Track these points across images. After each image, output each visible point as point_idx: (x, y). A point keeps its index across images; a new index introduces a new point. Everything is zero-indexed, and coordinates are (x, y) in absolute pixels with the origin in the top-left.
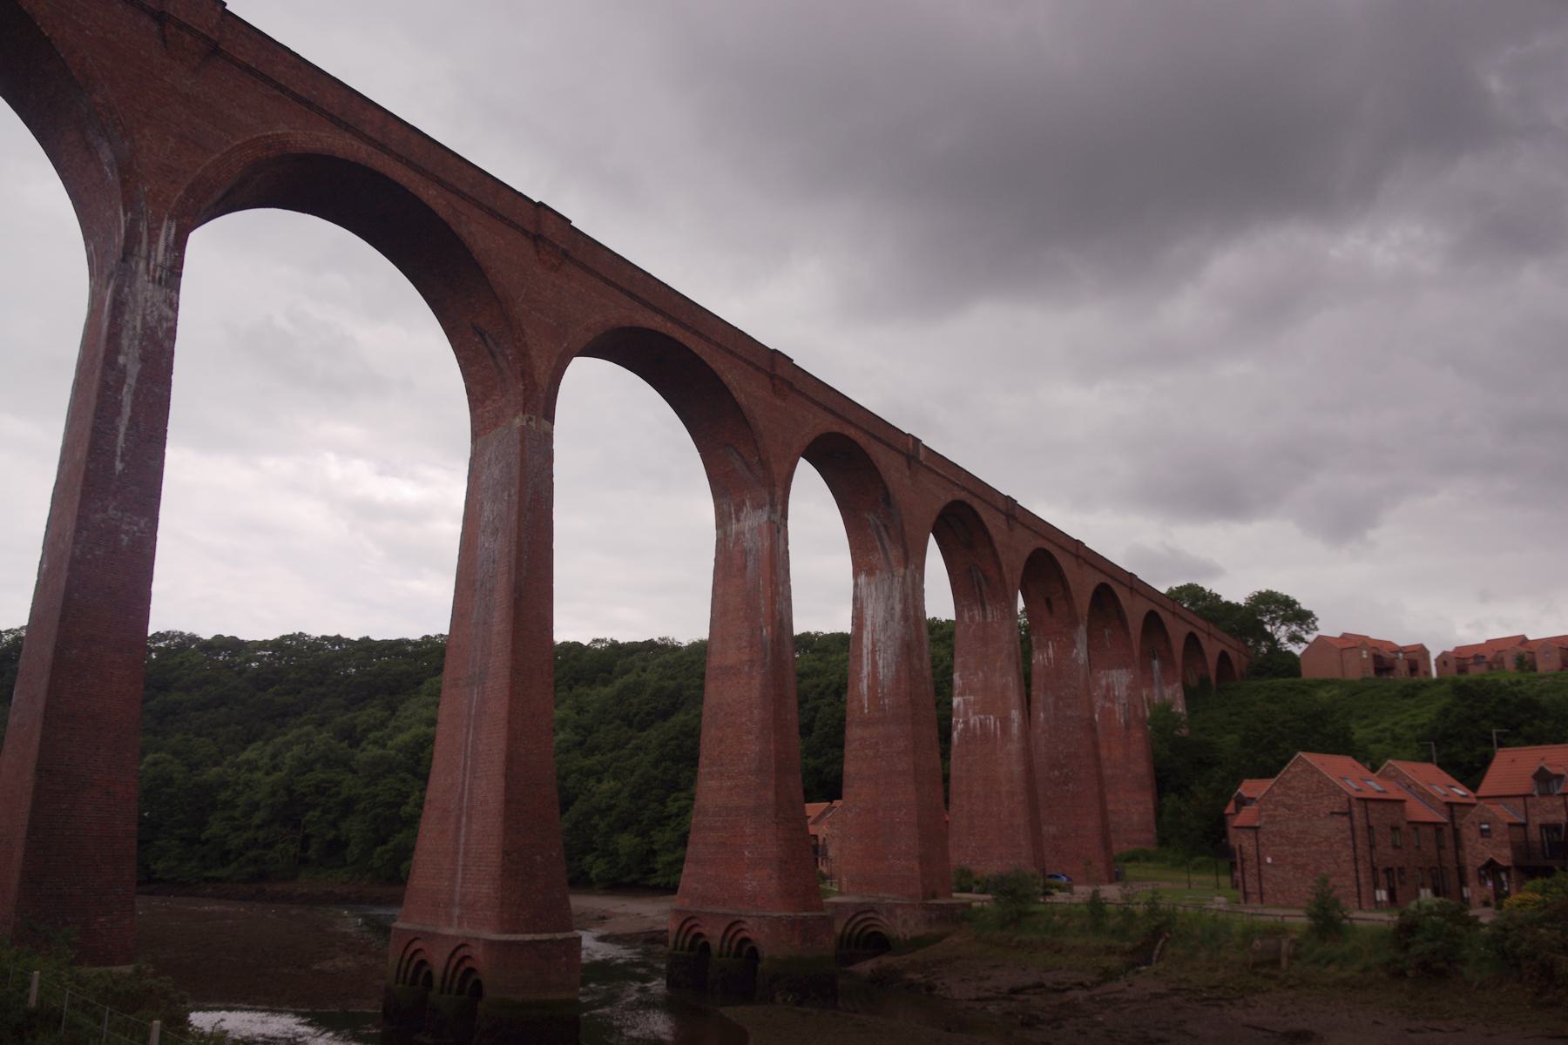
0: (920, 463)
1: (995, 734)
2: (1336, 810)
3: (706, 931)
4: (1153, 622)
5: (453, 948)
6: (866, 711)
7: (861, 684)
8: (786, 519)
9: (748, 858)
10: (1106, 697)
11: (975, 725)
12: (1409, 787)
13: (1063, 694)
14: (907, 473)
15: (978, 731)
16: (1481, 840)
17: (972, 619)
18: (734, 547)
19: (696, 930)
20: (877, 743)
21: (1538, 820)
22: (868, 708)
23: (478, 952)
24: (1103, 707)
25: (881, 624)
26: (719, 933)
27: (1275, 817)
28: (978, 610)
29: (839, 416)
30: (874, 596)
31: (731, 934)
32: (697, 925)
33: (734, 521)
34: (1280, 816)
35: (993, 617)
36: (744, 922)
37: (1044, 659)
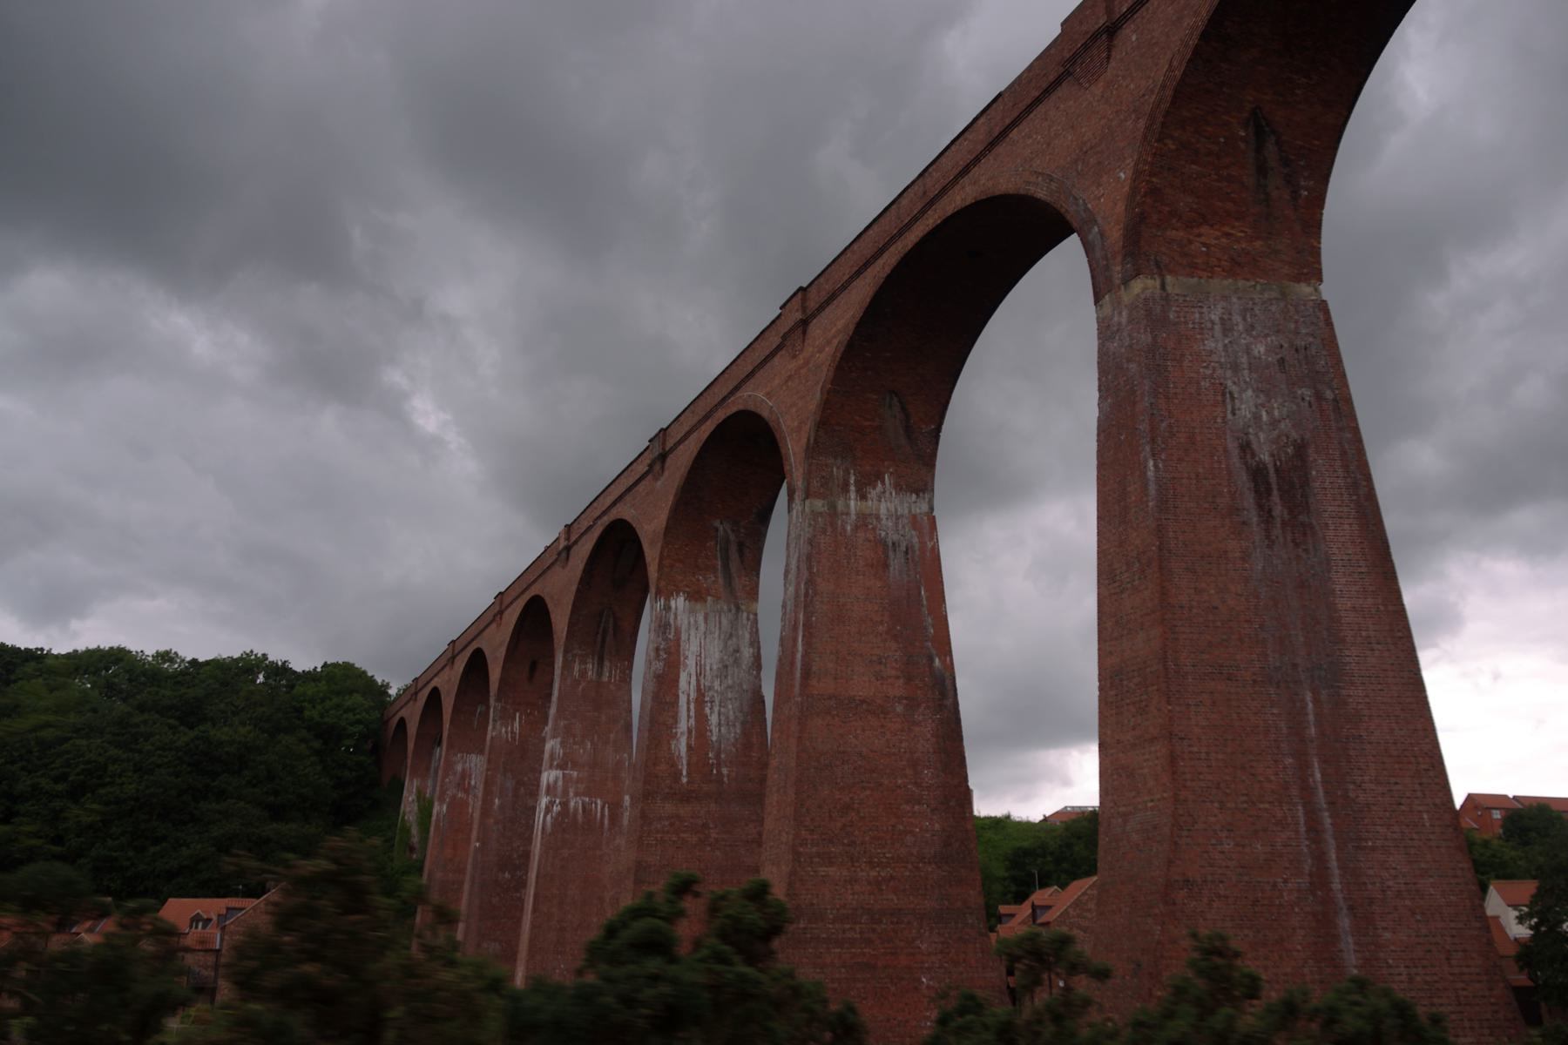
1: (602, 823)
6: (685, 780)
7: (673, 743)
9: (928, 987)
11: (576, 810)
13: (526, 779)
15: (580, 817)
17: (583, 673)
20: (705, 826)
22: (689, 774)
25: (715, 667)
28: (593, 664)
33: (853, 495)
35: (610, 677)
37: (506, 732)
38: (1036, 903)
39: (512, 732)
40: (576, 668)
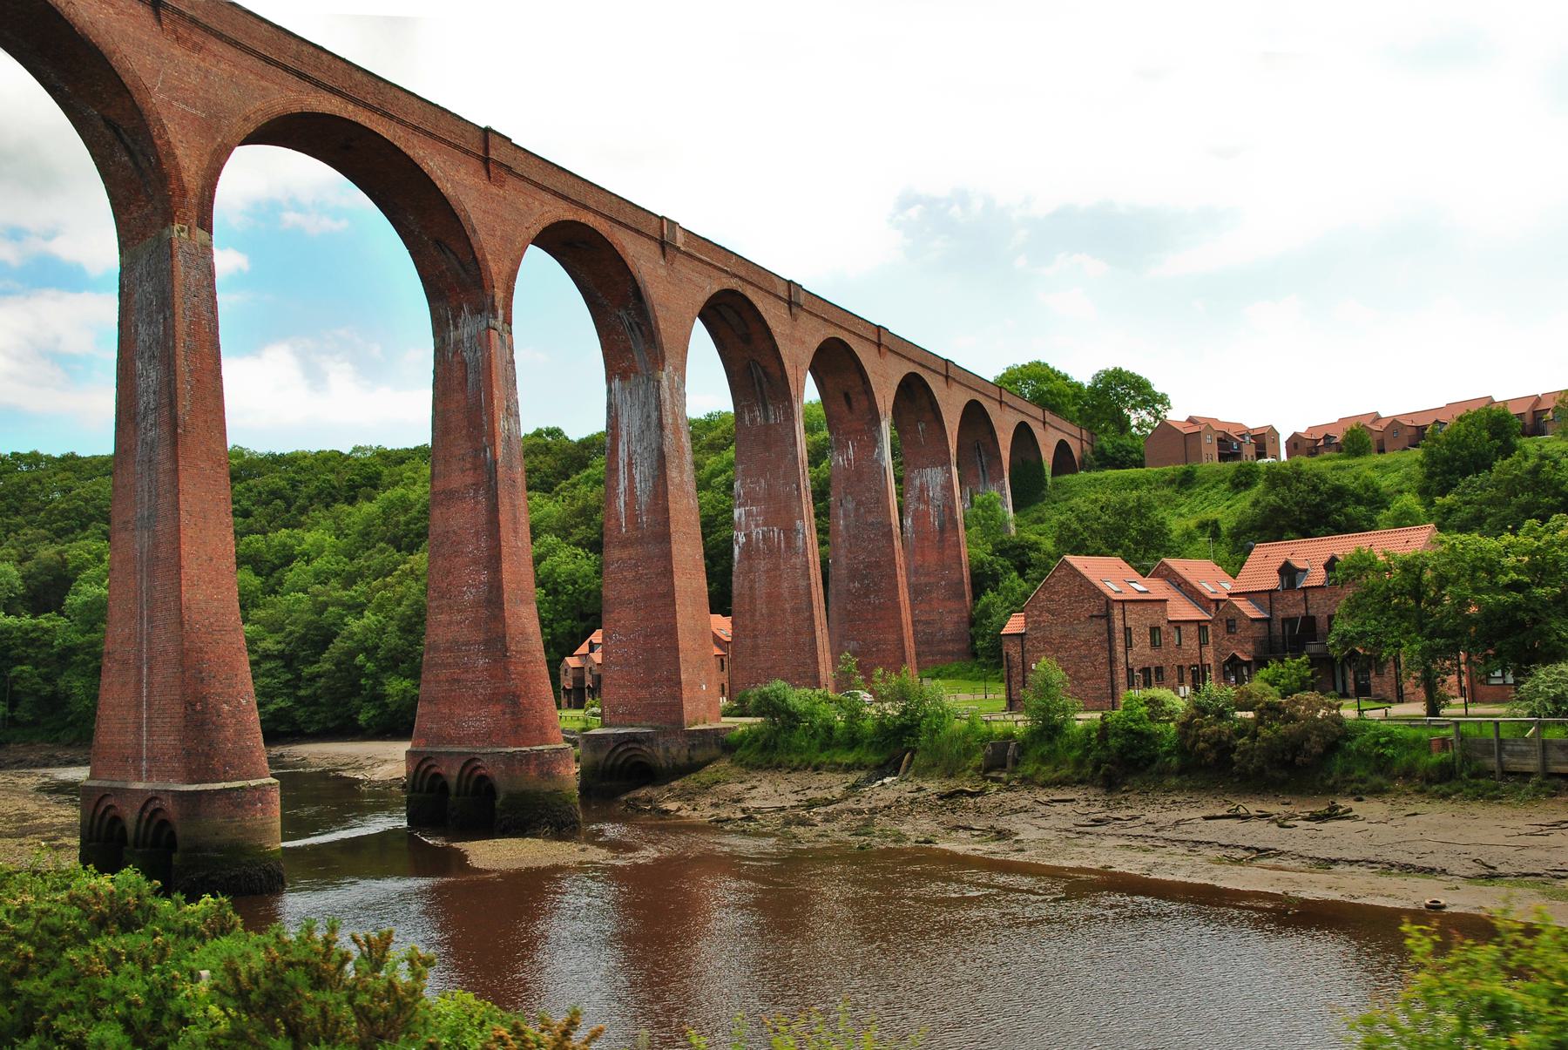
0: (678, 249)
1: (779, 547)
2: (1095, 613)
3: (443, 770)
4: (974, 415)
5: (143, 802)
6: (624, 530)
8: (510, 324)
10: (919, 499)
12: (1179, 585)
14: (662, 262)
16: (1227, 637)
17: (753, 421)
18: (453, 357)
19: (433, 770)
21: (1281, 614)
23: (168, 804)
24: (917, 509)
26: (455, 772)
27: (1040, 622)
29: (573, 202)
30: (629, 403)
31: (467, 771)
32: (433, 766)
34: (1044, 621)
35: (776, 418)
36: (479, 760)
38: (594, 641)
39: (848, 459)
40: (747, 418)
